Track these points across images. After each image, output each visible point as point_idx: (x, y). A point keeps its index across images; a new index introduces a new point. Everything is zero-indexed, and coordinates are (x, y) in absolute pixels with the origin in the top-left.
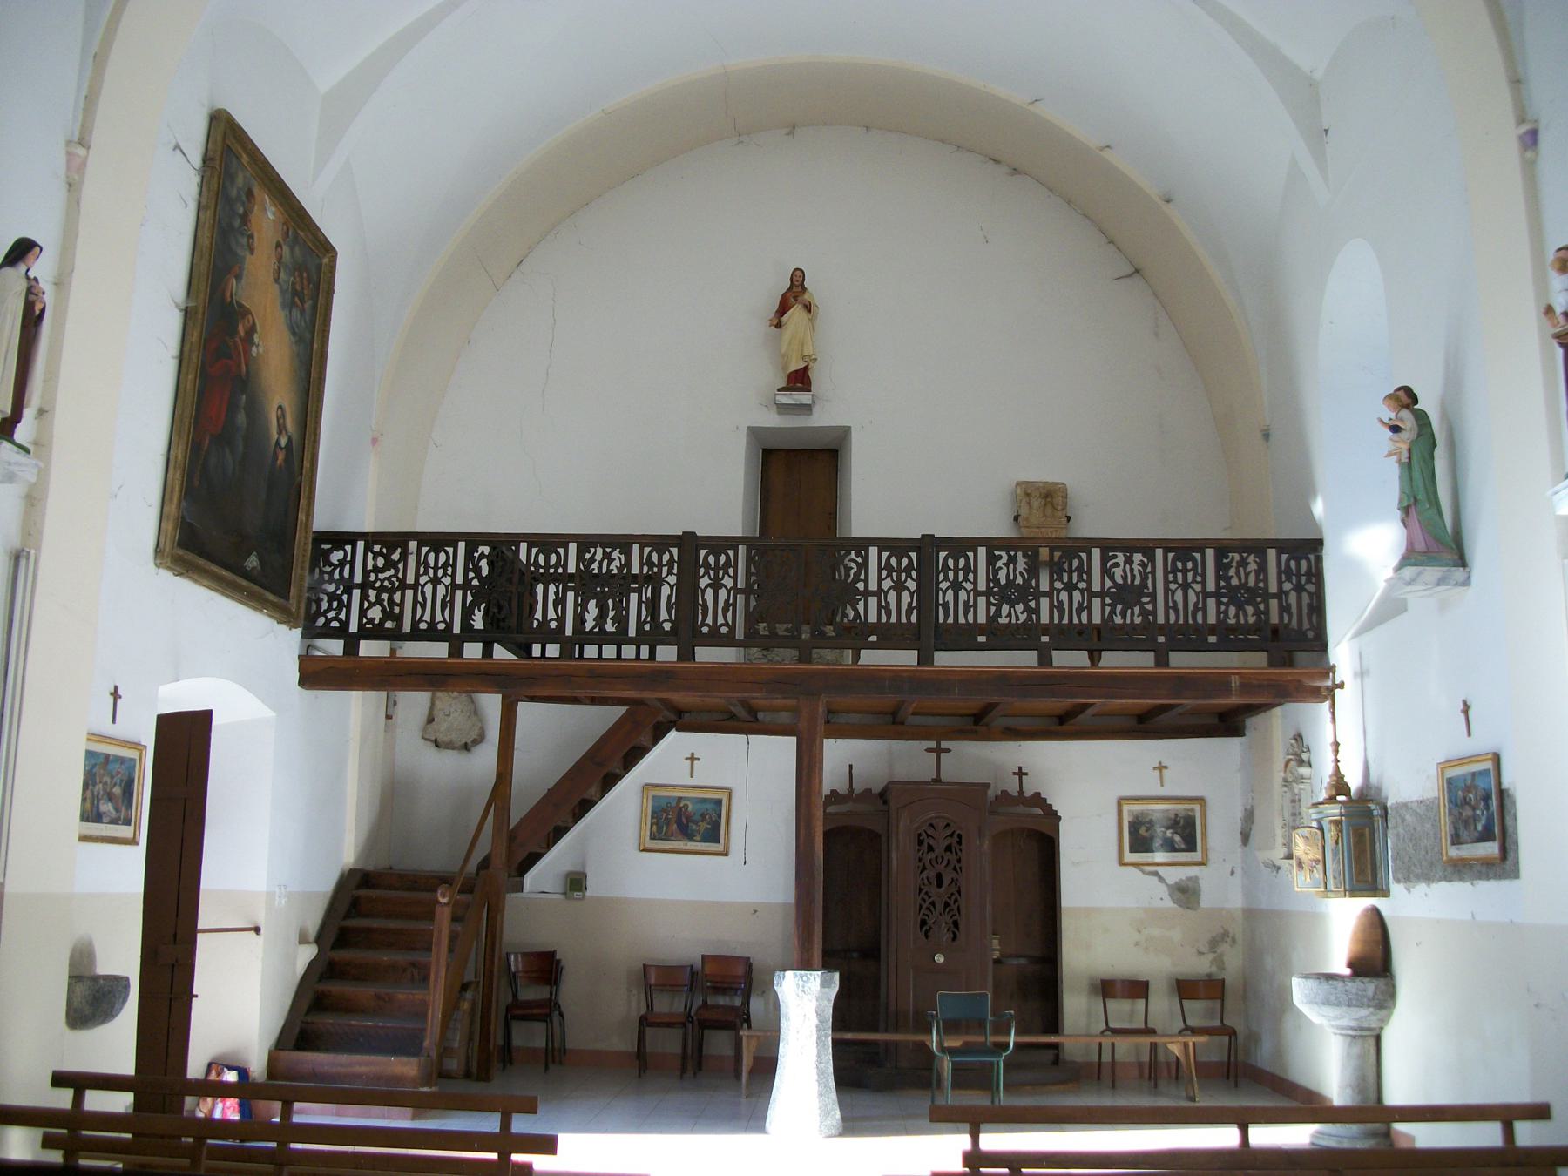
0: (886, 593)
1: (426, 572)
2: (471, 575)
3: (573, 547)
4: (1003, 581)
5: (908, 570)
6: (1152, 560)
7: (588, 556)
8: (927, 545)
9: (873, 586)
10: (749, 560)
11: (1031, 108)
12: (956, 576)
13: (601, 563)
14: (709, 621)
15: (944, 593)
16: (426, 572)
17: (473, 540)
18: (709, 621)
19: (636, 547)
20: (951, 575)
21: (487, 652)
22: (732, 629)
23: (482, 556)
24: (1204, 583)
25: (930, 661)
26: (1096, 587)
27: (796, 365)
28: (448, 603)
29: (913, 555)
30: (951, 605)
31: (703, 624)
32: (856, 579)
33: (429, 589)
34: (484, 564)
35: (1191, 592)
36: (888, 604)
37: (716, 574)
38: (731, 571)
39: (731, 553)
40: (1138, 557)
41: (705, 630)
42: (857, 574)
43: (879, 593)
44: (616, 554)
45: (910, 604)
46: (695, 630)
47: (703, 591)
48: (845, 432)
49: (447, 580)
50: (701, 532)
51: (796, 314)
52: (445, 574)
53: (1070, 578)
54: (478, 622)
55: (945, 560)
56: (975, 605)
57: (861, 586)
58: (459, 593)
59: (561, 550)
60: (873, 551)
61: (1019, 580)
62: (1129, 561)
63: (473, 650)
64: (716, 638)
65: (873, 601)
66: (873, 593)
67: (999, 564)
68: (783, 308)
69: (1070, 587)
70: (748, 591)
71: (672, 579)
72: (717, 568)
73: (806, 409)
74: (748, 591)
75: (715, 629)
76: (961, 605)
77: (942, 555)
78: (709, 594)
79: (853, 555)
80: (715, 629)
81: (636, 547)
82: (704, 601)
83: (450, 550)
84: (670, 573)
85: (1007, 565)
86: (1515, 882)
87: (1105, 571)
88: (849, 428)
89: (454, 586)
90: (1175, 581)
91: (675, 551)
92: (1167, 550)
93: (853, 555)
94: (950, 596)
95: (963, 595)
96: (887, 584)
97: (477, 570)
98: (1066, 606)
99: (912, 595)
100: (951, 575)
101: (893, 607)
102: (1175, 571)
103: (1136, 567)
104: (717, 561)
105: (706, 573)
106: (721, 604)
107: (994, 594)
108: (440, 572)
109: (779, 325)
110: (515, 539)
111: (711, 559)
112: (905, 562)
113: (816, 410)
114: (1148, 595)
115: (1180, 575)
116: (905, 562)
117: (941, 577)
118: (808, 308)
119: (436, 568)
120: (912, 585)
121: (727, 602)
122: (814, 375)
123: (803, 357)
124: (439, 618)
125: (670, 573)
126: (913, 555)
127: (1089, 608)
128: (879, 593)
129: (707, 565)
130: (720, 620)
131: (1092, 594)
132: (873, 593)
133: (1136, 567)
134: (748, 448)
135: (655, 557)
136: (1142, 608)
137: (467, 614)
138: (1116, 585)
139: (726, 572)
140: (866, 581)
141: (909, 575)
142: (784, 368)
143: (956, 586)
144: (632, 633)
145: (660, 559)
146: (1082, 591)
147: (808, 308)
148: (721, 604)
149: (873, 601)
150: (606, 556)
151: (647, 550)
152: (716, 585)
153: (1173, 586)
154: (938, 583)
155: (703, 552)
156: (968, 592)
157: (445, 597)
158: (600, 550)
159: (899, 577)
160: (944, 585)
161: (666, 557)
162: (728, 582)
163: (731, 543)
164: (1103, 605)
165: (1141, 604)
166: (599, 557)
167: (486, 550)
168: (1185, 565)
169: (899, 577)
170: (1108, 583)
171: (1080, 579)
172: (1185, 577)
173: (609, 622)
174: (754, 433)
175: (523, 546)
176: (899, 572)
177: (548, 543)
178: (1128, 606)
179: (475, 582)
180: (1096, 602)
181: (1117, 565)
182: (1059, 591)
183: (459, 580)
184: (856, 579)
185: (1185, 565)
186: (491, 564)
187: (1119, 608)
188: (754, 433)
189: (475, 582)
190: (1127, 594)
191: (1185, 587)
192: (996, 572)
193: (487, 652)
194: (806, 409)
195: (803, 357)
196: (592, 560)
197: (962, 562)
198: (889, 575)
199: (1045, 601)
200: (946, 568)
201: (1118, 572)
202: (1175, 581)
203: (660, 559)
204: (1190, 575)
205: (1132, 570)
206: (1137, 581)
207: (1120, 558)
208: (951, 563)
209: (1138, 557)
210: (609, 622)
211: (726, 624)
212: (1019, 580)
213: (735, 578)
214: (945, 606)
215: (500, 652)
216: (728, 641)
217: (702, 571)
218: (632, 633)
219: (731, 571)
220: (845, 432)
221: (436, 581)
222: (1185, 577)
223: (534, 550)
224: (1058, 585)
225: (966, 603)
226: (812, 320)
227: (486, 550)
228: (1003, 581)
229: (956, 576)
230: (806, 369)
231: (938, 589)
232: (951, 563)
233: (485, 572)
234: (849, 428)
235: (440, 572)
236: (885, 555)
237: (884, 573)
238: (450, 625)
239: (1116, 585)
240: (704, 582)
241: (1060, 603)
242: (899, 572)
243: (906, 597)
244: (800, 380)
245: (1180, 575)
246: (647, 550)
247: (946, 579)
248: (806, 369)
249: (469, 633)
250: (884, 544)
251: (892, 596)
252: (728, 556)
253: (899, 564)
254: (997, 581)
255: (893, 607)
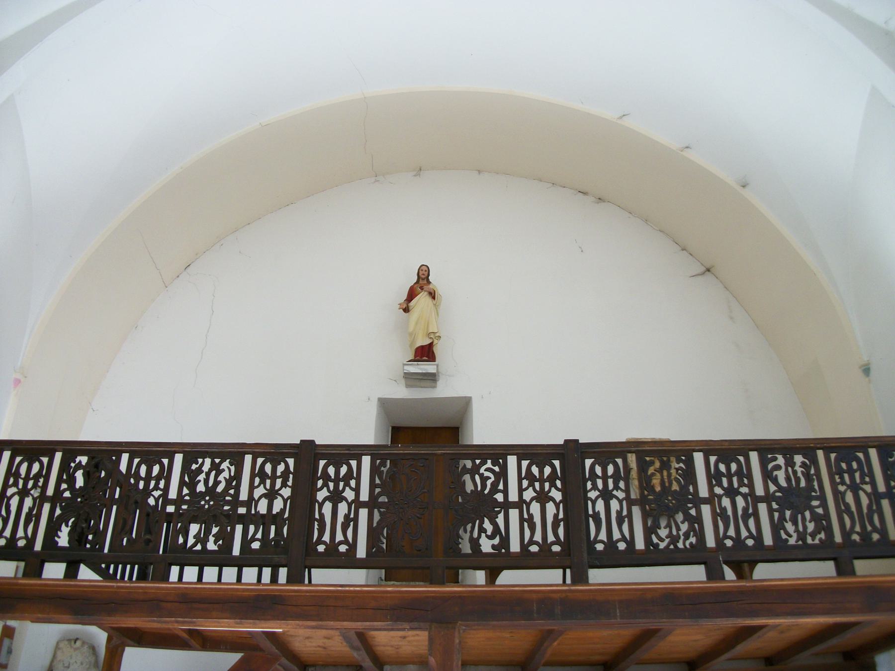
0: (528, 505)
1: (16, 484)
2: (64, 486)
3: (179, 458)
4: (658, 489)
5: (552, 479)
6: (815, 461)
7: (194, 467)
8: (572, 453)
9: (513, 497)
10: (374, 470)
12: (605, 484)
13: (208, 474)
14: (326, 538)
15: (594, 502)
16: (16, 484)
17: (71, 449)
18: (326, 538)
19: (248, 459)
20: (600, 483)
21: (71, 572)
22: (353, 547)
23: (79, 466)
24: (873, 483)
25: (584, 579)
26: (760, 491)
28: (33, 517)
29: (557, 463)
30: (603, 516)
31: (320, 541)
32: (494, 489)
33: (15, 502)
34: (79, 475)
35: (861, 493)
36: (531, 516)
37: (336, 486)
38: (353, 483)
39: (354, 463)
40: (798, 459)
41: (321, 548)
42: (495, 485)
43: (521, 504)
44: (225, 465)
45: (556, 516)
46: (310, 548)
47: (321, 505)
49: (36, 493)
50: (320, 440)
52: (35, 486)
53: (730, 482)
54: (63, 539)
55: (592, 467)
56: (630, 516)
57: (499, 497)
58: (47, 507)
59: (166, 461)
60: (512, 460)
61: (675, 487)
62: (790, 463)
63: (54, 571)
64: (336, 559)
65: (514, 514)
66: (514, 505)
67: (651, 470)
69: (731, 493)
70: (371, 505)
71: (286, 492)
72: (337, 480)
73: (431, 378)
74: (371, 505)
75: (332, 546)
76: (614, 515)
77: (588, 462)
78: (327, 508)
79: (489, 464)
80: (332, 546)
81: (248, 459)
82: (322, 515)
83: (45, 460)
84: (284, 485)
85: (660, 471)
87: (768, 476)
89: (43, 498)
90: (843, 483)
91: (291, 461)
92: (828, 450)
93: (489, 464)
94: (600, 506)
95: (614, 505)
96: (529, 495)
97: (72, 480)
98: (730, 512)
99: (557, 506)
100: (600, 483)
101: (537, 519)
102: (840, 473)
103: (799, 470)
104: (337, 472)
105: (325, 485)
106: (340, 519)
107: (649, 502)
108: (30, 484)
110: (113, 450)
111: (331, 470)
112: (547, 470)
114: (816, 498)
115: (846, 476)
116: (547, 470)
117: (589, 485)
118: (433, 295)
119: (27, 479)
120: (557, 495)
121: (347, 517)
124: (20, 533)
125: (284, 485)
126: (557, 463)
127: (756, 515)
128: (521, 504)
129: (326, 477)
130: (339, 537)
131: (757, 500)
132: (514, 505)
133: (799, 470)
135: (268, 468)
136: (813, 513)
137: (53, 529)
138: (780, 488)
139: (347, 484)
140: (505, 492)
141: (552, 485)
143: (606, 495)
144: (236, 551)
145: (274, 470)
146: (745, 496)
147: (433, 295)
148: (340, 519)
149: (514, 514)
150: (216, 467)
151: (260, 461)
152: (336, 498)
153: (842, 488)
154: (586, 492)
155: (322, 463)
156: (620, 502)
157: (31, 510)
158: (208, 461)
159: (542, 487)
160: (593, 495)
161: (281, 468)
162: (349, 495)
163: (354, 452)
164: (771, 511)
165: (812, 509)
166: (206, 468)
167: (84, 460)
168: (849, 466)
169: (542, 487)
170: (772, 488)
171: (741, 484)
172: (852, 478)
173: (212, 539)
175: (125, 457)
176: (542, 481)
177: (152, 453)
178: (798, 511)
179: (67, 494)
180: (762, 508)
181: (778, 467)
182: (720, 497)
183: (50, 492)
184: (494, 489)
185: (849, 466)
186: (87, 476)
187: (788, 513)
189: (67, 494)
190: (793, 499)
191: (855, 488)
192: (649, 478)
193: (71, 572)
194: (431, 378)
196: (199, 471)
197: (611, 469)
198: (531, 484)
199: (706, 510)
200: (593, 476)
201: (781, 475)
202: (843, 483)
203: (274, 470)
204: (857, 475)
205: (795, 472)
206: (803, 484)
207: (781, 460)
208: (598, 470)
209: (798, 459)
210: (212, 539)
211: (345, 541)
212: (675, 487)
213: (357, 490)
214: (596, 517)
215: (86, 573)
216: (349, 561)
217: (320, 483)
218: (236, 551)
219: (353, 483)
221: (24, 493)
222: (852, 478)
223: (136, 461)
224: (718, 491)
225: (619, 513)
227: (84, 460)
228: (658, 489)
229: (605, 484)
230: (431, 345)
231: (587, 499)
232: (598, 470)
233: (80, 482)
235: (30, 484)
236: (525, 464)
237: (525, 483)
238: (31, 541)
239: (780, 488)
240: (321, 495)
241: (724, 510)
242: (542, 481)
243: (550, 508)
245: (846, 476)
246: (260, 461)
247: (595, 487)
248: (431, 345)
249: (52, 552)
250: (525, 452)
251: (535, 508)
252: (350, 468)
253: (541, 472)
254: (651, 489)
255: (537, 519)
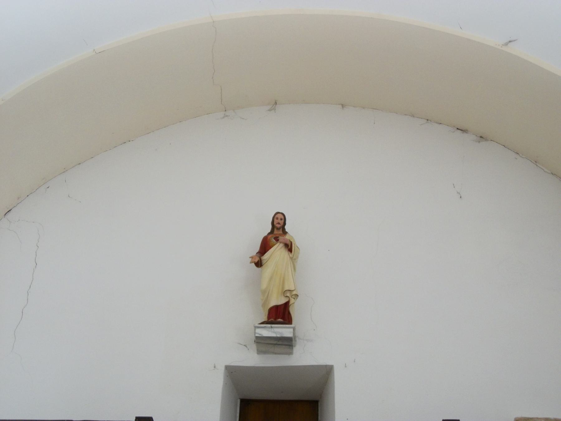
11: (505, 49)
27: (277, 300)
48: (326, 373)
51: (277, 252)
68: (265, 247)
86: (228, 364)
88: (227, 368)
109: (259, 264)
113: (297, 349)
118: (289, 247)
122: (294, 311)
123: (284, 293)
134: (225, 384)
142: (264, 305)
147: (289, 247)
174: (233, 373)
188: (233, 373)
195: (284, 293)
220: (326, 373)
226: (293, 260)
234: (227, 368)
244: (280, 314)
